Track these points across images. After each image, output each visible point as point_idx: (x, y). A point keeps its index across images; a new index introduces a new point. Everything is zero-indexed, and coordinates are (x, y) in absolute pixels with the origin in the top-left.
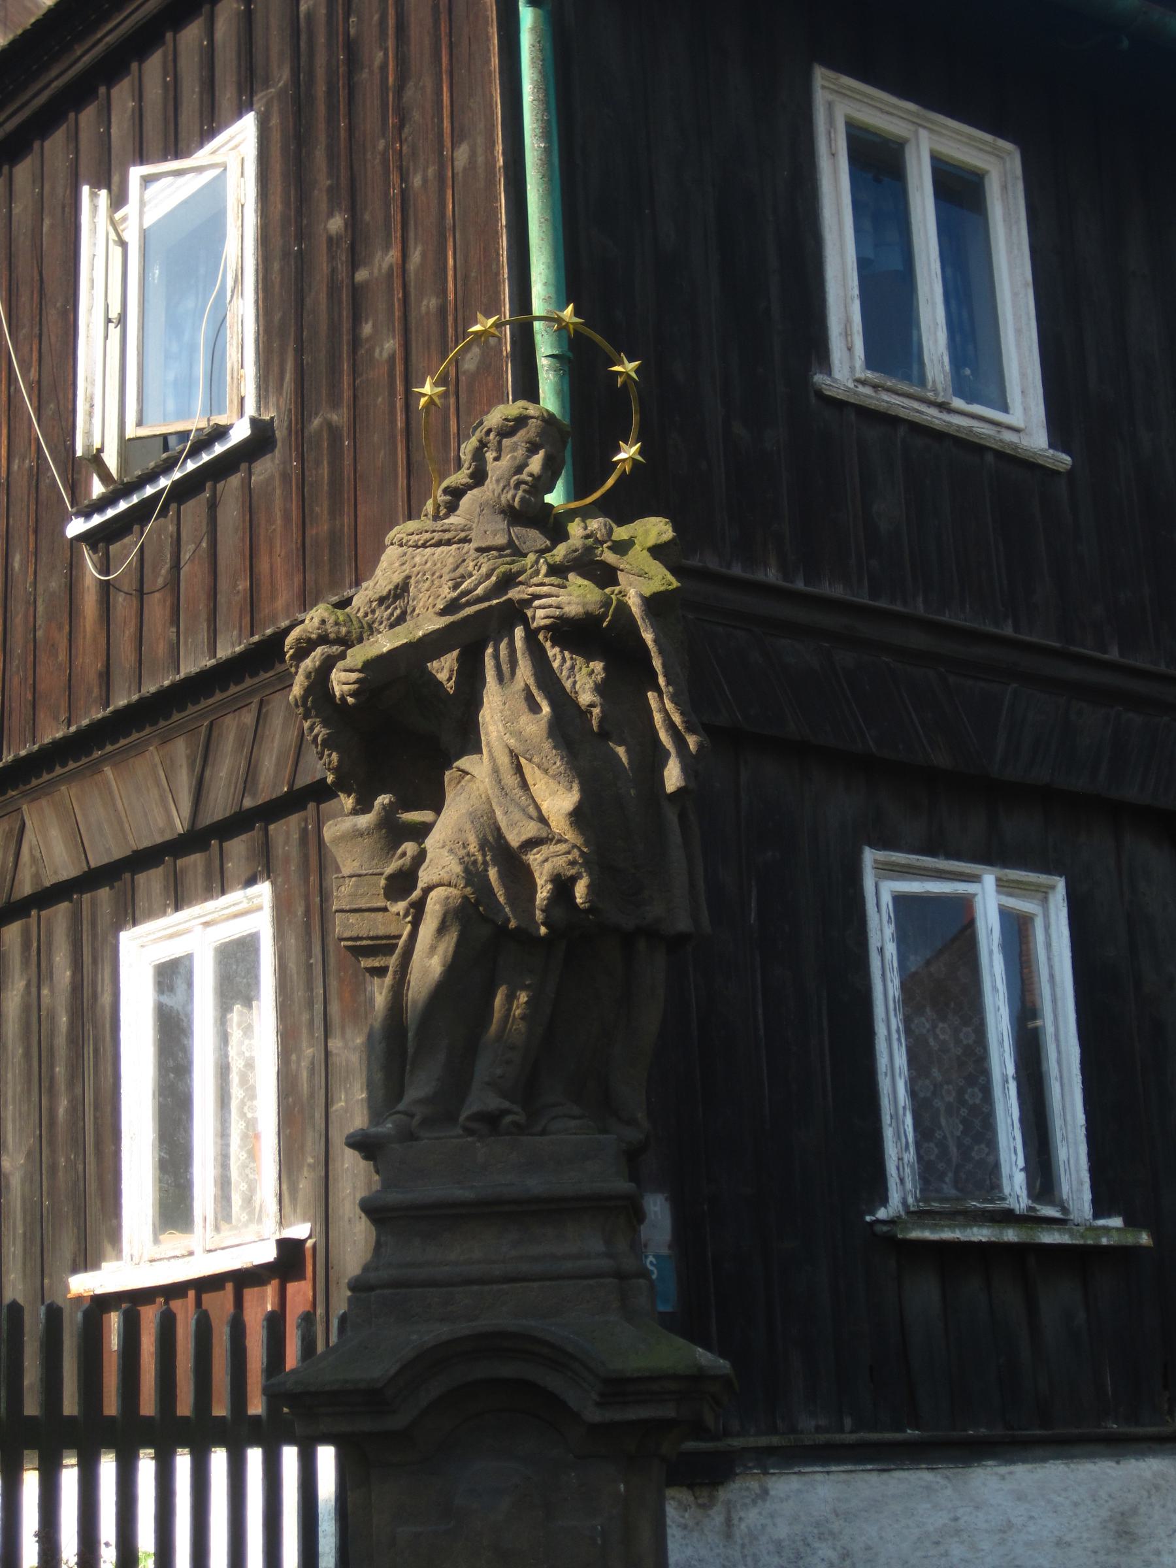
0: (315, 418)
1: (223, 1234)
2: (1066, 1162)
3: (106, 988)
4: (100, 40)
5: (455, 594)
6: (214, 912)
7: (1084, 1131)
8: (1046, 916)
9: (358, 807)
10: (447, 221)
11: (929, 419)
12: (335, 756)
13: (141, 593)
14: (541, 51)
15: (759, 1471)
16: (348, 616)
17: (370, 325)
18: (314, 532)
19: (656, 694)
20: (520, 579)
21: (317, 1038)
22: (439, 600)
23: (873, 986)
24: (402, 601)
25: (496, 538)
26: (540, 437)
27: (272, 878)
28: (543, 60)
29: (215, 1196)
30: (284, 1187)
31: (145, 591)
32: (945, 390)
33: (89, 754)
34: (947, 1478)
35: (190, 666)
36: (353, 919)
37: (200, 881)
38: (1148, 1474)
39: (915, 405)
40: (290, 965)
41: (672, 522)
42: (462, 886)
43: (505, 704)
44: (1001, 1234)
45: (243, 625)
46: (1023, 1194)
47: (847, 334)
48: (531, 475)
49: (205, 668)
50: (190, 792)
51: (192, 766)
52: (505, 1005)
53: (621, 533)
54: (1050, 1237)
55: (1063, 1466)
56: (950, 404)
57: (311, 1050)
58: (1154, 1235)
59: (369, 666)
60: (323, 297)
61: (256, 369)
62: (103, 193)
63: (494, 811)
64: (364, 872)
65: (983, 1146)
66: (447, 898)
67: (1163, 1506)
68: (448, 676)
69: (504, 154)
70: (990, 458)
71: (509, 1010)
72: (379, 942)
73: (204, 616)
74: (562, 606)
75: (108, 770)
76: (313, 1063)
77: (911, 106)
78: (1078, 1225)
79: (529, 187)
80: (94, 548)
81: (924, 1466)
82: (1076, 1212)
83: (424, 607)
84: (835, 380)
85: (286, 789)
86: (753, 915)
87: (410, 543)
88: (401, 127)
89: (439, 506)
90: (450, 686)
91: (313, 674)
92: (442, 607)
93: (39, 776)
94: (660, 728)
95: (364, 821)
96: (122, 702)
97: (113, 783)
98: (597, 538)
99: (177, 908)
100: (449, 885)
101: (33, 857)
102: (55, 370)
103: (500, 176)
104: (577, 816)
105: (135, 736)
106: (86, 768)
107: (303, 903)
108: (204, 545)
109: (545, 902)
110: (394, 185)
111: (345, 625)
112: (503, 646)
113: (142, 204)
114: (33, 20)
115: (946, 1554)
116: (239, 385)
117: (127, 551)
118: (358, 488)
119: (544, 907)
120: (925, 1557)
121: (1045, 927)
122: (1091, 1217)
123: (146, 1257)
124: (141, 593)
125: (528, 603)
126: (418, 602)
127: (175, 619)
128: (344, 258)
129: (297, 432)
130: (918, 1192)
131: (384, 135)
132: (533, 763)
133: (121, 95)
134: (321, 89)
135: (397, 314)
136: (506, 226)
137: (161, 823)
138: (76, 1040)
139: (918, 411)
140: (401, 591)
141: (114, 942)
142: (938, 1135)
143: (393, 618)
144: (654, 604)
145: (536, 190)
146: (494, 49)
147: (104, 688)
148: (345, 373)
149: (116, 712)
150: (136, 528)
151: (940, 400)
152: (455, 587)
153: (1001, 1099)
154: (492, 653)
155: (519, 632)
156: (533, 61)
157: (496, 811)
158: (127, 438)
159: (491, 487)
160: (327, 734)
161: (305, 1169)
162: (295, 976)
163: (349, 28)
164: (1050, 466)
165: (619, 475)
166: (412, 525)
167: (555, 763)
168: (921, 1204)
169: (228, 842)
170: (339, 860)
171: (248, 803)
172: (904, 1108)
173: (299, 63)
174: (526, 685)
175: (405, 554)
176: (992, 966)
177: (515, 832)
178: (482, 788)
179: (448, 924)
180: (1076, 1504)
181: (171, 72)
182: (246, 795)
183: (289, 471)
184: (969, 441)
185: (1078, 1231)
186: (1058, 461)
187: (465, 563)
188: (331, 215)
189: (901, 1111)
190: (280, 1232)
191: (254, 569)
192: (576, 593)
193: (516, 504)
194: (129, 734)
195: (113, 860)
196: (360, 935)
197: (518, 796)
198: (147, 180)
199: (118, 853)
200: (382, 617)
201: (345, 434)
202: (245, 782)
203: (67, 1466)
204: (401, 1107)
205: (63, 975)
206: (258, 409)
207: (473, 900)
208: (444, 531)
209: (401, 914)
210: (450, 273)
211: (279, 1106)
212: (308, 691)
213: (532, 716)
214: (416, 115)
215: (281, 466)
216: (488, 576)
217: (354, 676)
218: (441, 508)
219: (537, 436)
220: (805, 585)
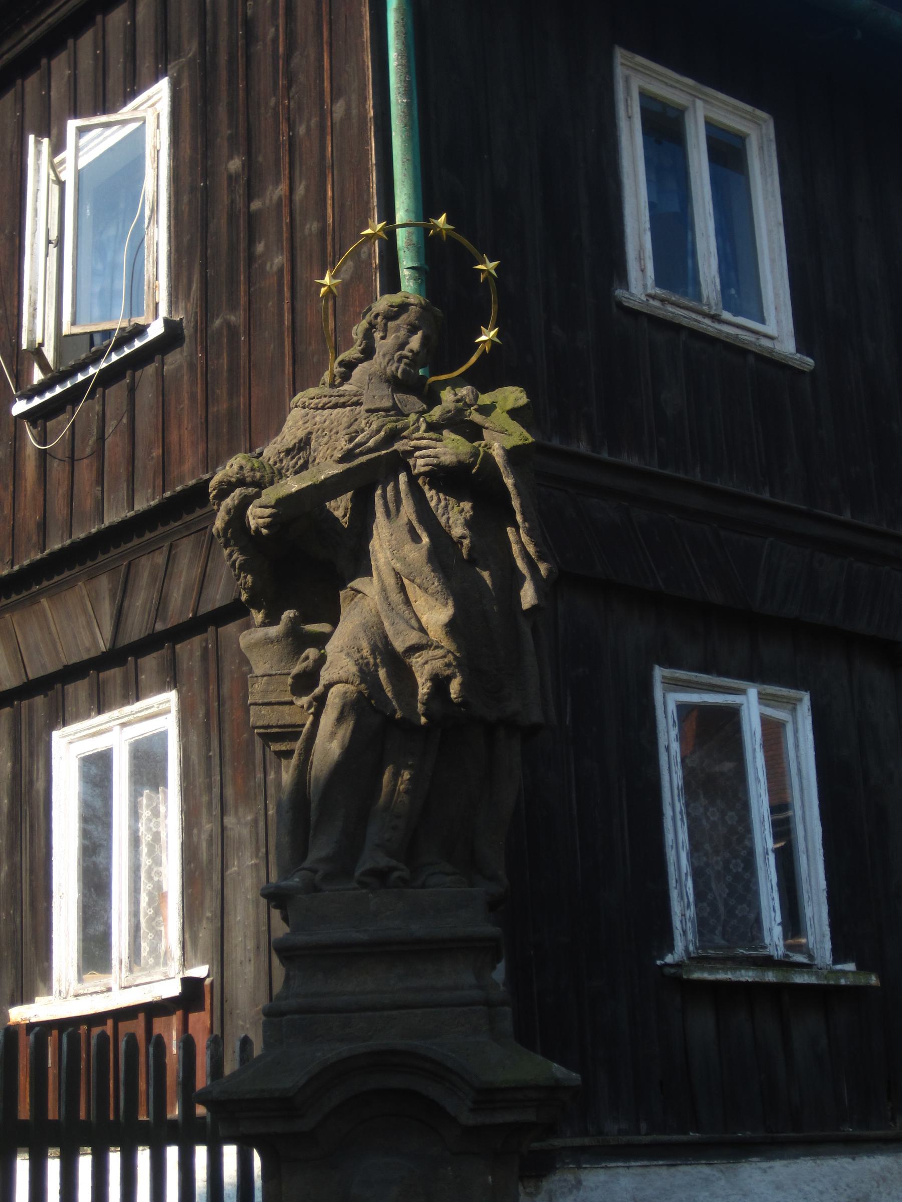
0: (217, 319)
1: (135, 974)
2: (812, 919)
3: (40, 776)
4: (43, 21)
6: (129, 715)
7: (825, 894)
8: (795, 723)
9: (267, 621)
10: (327, 161)
11: (705, 327)
12: (249, 578)
13: (72, 459)
14: (404, 26)
15: (574, 1166)
16: (262, 463)
17: (262, 244)
18: (215, 409)
19: (513, 529)
20: (404, 434)
21: (215, 815)
22: (336, 451)
23: (662, 776)
24: (305, 452)
25: (382, 402)
26: (419, 321)
27: (178, 687)
28: (405, 34)
29: (129, 943)
30: (187, 936)
31: (75, 459)
32: (717, 305)
33: (29, 588)
34: (722, 1171)
35: (111, 518)
36: (265, 710)
37: (118, 691)
38: (877, 1168)
40: (192, 757)
41: (525, 390)
42: (358, 683)
43: (392, 535)
45: (156, 484)
47: (640, 259)
48: (411, 351)
49: (126, 518)
50: (111, 618)
51: (113, 597)
52: (391, 781)
53: (485, 399)
54: (801, 979)
55: (811, 1162)
56: (720, 315)
57: (210, 825)
58: (881, 977)
59: (283, 503)
60: (224, 222)
61: (169, 280)
62: (46, 141)
63: (382, 623)
64: (274, 672)
65: (745, 906)
66: (346, 693)
67: (889, 1194)
68: (343, 513)
69: (374, 107)
70: (751, 359)
71: (395, 785)
72: (286, 730)
73: (124, 478)
74: (439, 456)
75: (44, 602)
76: (211, 836)
78: (821, 969)
79: (394, 134)
80: (34, 424)
81: (704, 1162)
82: (819, 958)
83: (323, 457)
84: (632, 295)
85: (191, 615)
86: (568, 719)
87: (312, 405)
88: (289, 86)
89: (335, 376)
90: (345, 522)
91: (232, 511)
92: (340, 456)
94: (518, 556)
95: (274, 631)
96: (57, 546)
97: (48, 611)
98: (466, 402)
99: (100, 712)
100: (347, 682)
102: (3, 283)
103: (371, 124)
104: (452, 627)
105: (67, 573)
106: (26, 599)
107: (203, 707)
108: (125, 421)
109: (426, 697)
110: (283, 133)
111: (259, 471)
112: (390, 488)
113: (77, 149)
116: (154, 293)
118: (252, 374)
119: (424, 701)
121: (794, 731)
122: (831, 962)
123: (72, 992)
124: (72, 459)
125: (410, 453)
126: (318, 454)
127: (100, 480)
128: (241, 192)
129: (202, 331)
130: (697, 942)
131: (275, 95)
132: (415, 584)
133: (60, 65)
134: (223, 58)
135: (285, 235)
136: (376, 164)
137: (87, 643)
139: (696, 321)
140: (304, 444)
141: (47, 739)
142: (709, 896)
143: (297, 467)
144: (514, 455)
145: (399, 136)
146: (366, 24)
147: (41, 534)
148: (242, 283)
149: (51, 554)
150: (69, 408)
151: (713, 312)
152: (351, 440)
153: (763, 868)
154: (381, 494)
155: (403, 478)
157: (385, 623)
158: (63, 335)
159: (378, 361)
160: (243, 560)
161: (204, 921)
162: (197, 767)
163: (246, 9)
164: (798, 367)
165: (480, 353)
166: (312, 391)
167: (434, 583)
168: (699, 951)
169: (142, 659)
170: (252, 663)
171: (159, 627)
172: (686, 874)
173: (205, 38)
174: (409, 520)
175: (307, 415)
176: (755, 761)
177: (400, 639)
178: (372, 604)
180: (821, 1193)
182: (158, 620)
183: (195, 362)
184: (735, 345)
185: (823, 974)
186: (804, 363)
187: (358, 421)
188: (231, 157)
189: (684, 877)
190: (183, 972)
191: (166, 440)
192: (450, 446)
193: (399, 374)
194: (61, 573)
195: (46, 674)
196: (270, 724)
197: (402, 610)
199: (51, 669)
200: (288, 466)
201: (242, 331)
202: (157, 610)
204: (306, 864)
206: (170, 312)
207: (366, 695)
208: (340, 396)
209: (305, 706)
210: (329, 202)
211: (183, 870)
212: (228, 525)
213: (413, 545)
214: (302, 78)
215: (189, 358)
216: (378, 431)
217: (268, 511)
218: (337, 378)
219: (416, 320)
220: (610, 455)
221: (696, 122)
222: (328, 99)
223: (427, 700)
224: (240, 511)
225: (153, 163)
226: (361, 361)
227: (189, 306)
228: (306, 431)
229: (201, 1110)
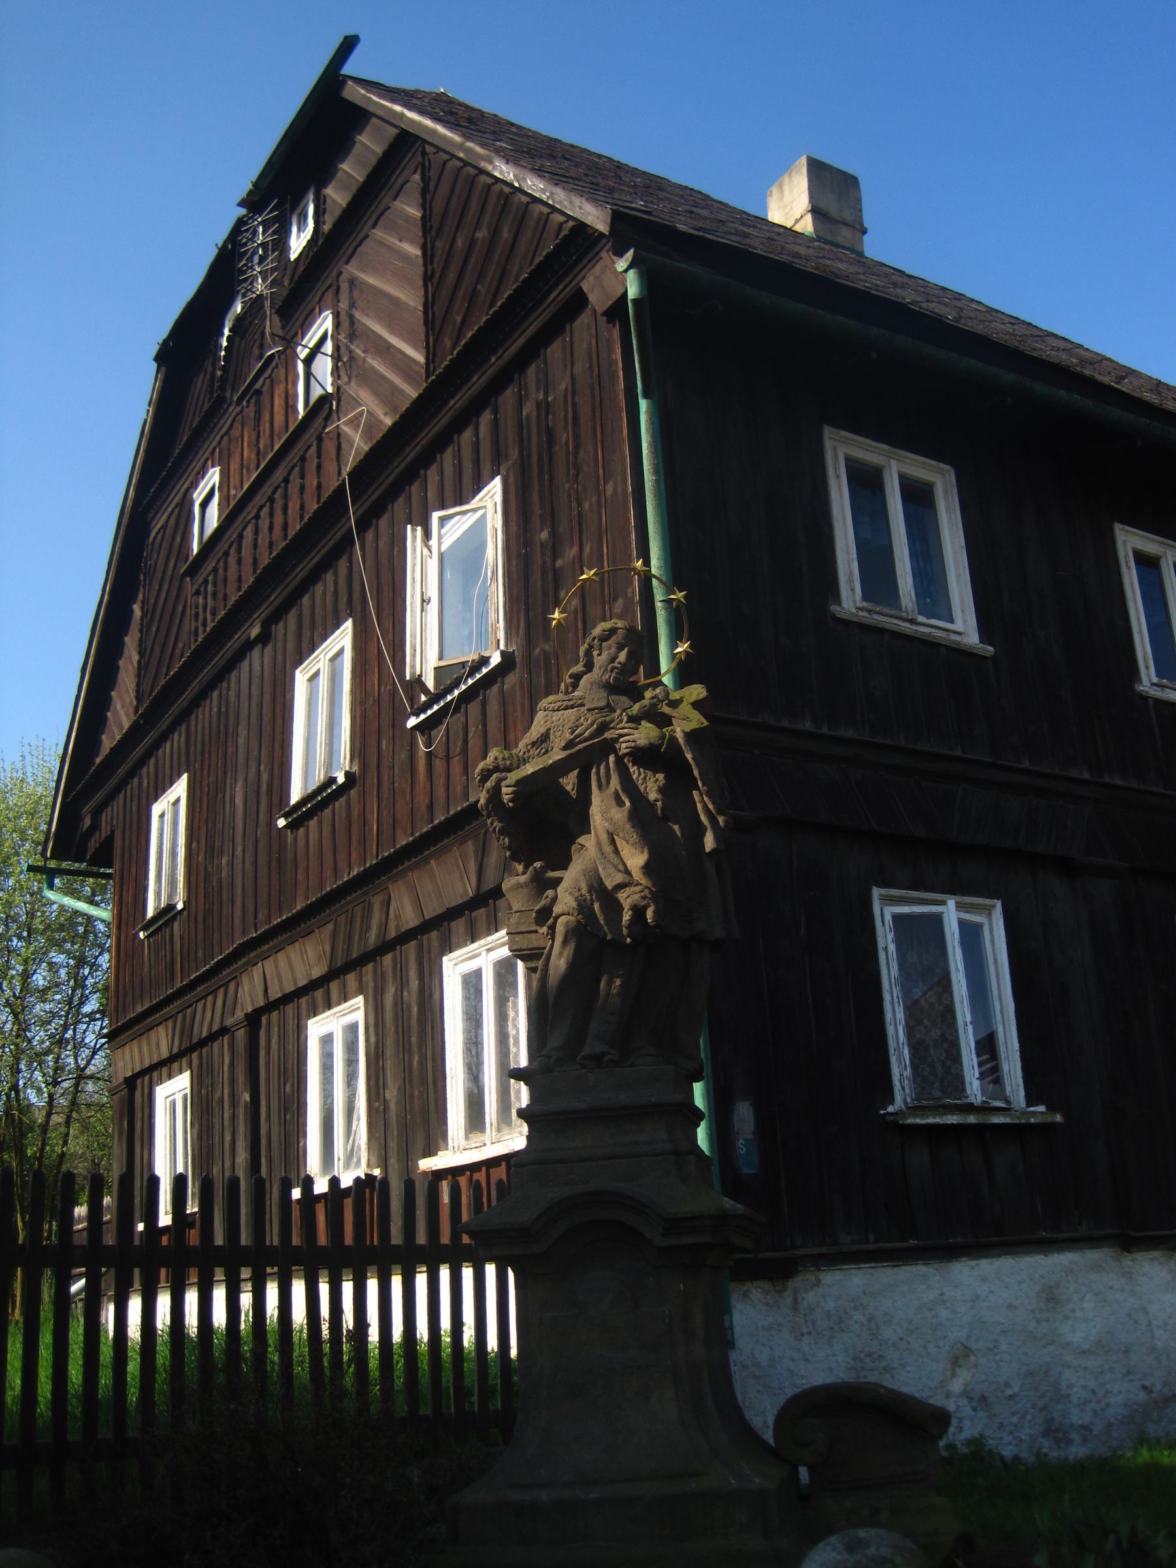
4: (418, 443)
5: (572, 737)
8: (991, 924)
12: (507, 840)
13: (448, 758)
28: (653, 429)
32: (913, 611)
34: (937, 1269)
38: (1066, 1263)
39: (895, 621)
44: (966, 1118)
46: (979, 1094)
47: (851, 581)
48: (620, 663)
58: (1064, 1116)
60: (539, 577)
67: (1076, 1282)
71: (610, 990)
75: (433, 862)
77: (886, 447)
80: (423, 734)
84: (843, 608)
90: (573, 794)
93: (397, 868)
99: (473, 942)
100: (568, 914)
101: (395, 915)
104: (647, 868)
105: (446, 841)
114: (381, 435)
115: (936, 1316)
116: (496, 633)
117: (440, 733)
120: (923, 1318)
124: (448, 758)
125: (616, 740)
133: (432, 474)
134: (535, 459)
138: (422, 1021)
139: (896, 624)
140: (545, 738)
142: (929, 1060)
144: (693, 737)
151: (910, 617)
152: (572, 733)
155: (612, 758)
156: (647, 430)
166: (551, 698)
172: (903, 1044)
175: (547, 716)
179: (569, 938)
180: (1020, 1283)
181: (457, 458)
188: (542, 530)
194: (443, 840)
198: (443, 521)
199: (439, 911)
202: (505, 864)
203: (420, 1272)
205: (414, 984)
206: (506, 645)
208: (569, 700)
210: (605, 557)
212: (488, 801)
214: (585, 468)
216: (592, 725)
217: (511, 789)
221: (891, 476)
222: (602, 482)
223: (629, 924)
224: (497, 789)
225: (492, 538)
226: (586, 674)
227: (519, 641)
228: (546, 728)
229: (466, 1239)
